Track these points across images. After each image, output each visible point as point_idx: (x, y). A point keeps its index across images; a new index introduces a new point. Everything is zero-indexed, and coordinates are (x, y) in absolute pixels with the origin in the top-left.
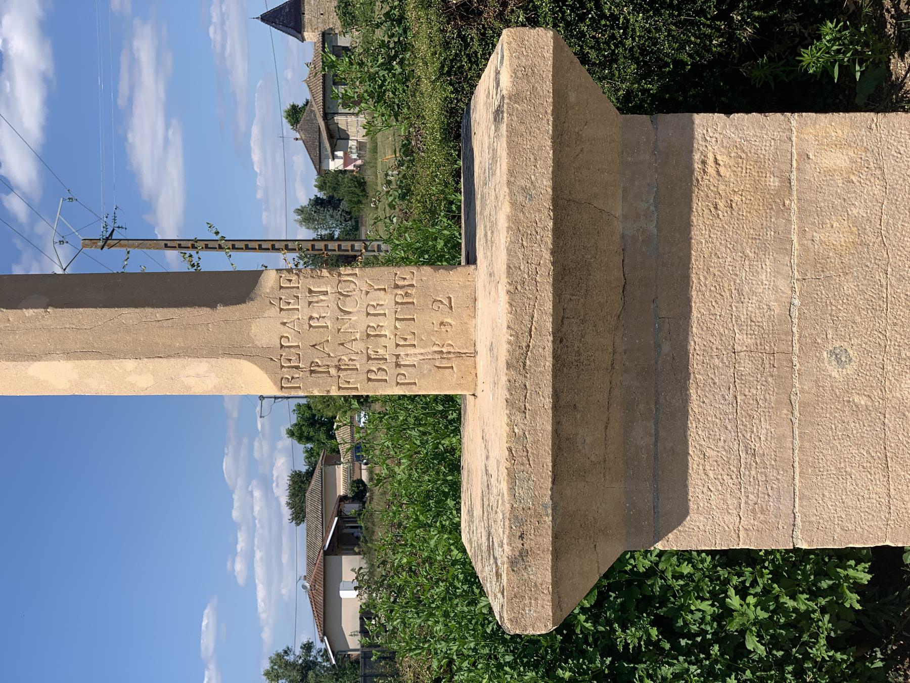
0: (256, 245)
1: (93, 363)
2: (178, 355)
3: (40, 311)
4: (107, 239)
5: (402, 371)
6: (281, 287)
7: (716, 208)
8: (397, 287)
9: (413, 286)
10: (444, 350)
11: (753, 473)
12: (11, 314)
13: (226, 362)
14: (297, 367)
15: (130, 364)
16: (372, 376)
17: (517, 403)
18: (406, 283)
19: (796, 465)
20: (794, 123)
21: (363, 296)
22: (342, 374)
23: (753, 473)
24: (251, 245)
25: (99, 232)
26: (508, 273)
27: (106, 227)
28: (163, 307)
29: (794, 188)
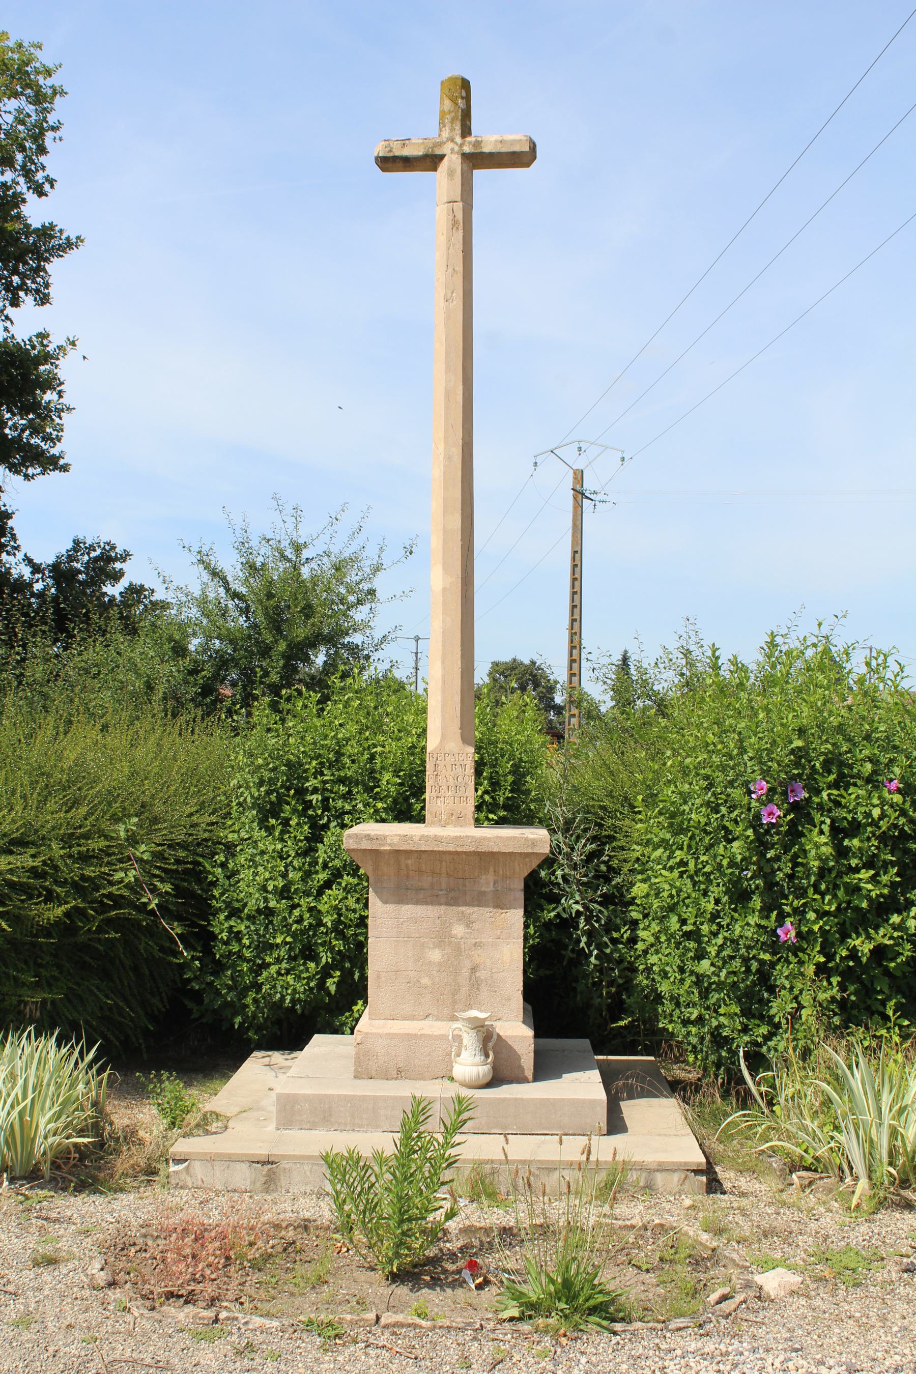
0: (577, 616)
1: (440, 685)
4: (583, 494)
15: (440, 698)
17: (423, 838)
24: (577, 611)
25: (589, 485)
27: (595, 493)
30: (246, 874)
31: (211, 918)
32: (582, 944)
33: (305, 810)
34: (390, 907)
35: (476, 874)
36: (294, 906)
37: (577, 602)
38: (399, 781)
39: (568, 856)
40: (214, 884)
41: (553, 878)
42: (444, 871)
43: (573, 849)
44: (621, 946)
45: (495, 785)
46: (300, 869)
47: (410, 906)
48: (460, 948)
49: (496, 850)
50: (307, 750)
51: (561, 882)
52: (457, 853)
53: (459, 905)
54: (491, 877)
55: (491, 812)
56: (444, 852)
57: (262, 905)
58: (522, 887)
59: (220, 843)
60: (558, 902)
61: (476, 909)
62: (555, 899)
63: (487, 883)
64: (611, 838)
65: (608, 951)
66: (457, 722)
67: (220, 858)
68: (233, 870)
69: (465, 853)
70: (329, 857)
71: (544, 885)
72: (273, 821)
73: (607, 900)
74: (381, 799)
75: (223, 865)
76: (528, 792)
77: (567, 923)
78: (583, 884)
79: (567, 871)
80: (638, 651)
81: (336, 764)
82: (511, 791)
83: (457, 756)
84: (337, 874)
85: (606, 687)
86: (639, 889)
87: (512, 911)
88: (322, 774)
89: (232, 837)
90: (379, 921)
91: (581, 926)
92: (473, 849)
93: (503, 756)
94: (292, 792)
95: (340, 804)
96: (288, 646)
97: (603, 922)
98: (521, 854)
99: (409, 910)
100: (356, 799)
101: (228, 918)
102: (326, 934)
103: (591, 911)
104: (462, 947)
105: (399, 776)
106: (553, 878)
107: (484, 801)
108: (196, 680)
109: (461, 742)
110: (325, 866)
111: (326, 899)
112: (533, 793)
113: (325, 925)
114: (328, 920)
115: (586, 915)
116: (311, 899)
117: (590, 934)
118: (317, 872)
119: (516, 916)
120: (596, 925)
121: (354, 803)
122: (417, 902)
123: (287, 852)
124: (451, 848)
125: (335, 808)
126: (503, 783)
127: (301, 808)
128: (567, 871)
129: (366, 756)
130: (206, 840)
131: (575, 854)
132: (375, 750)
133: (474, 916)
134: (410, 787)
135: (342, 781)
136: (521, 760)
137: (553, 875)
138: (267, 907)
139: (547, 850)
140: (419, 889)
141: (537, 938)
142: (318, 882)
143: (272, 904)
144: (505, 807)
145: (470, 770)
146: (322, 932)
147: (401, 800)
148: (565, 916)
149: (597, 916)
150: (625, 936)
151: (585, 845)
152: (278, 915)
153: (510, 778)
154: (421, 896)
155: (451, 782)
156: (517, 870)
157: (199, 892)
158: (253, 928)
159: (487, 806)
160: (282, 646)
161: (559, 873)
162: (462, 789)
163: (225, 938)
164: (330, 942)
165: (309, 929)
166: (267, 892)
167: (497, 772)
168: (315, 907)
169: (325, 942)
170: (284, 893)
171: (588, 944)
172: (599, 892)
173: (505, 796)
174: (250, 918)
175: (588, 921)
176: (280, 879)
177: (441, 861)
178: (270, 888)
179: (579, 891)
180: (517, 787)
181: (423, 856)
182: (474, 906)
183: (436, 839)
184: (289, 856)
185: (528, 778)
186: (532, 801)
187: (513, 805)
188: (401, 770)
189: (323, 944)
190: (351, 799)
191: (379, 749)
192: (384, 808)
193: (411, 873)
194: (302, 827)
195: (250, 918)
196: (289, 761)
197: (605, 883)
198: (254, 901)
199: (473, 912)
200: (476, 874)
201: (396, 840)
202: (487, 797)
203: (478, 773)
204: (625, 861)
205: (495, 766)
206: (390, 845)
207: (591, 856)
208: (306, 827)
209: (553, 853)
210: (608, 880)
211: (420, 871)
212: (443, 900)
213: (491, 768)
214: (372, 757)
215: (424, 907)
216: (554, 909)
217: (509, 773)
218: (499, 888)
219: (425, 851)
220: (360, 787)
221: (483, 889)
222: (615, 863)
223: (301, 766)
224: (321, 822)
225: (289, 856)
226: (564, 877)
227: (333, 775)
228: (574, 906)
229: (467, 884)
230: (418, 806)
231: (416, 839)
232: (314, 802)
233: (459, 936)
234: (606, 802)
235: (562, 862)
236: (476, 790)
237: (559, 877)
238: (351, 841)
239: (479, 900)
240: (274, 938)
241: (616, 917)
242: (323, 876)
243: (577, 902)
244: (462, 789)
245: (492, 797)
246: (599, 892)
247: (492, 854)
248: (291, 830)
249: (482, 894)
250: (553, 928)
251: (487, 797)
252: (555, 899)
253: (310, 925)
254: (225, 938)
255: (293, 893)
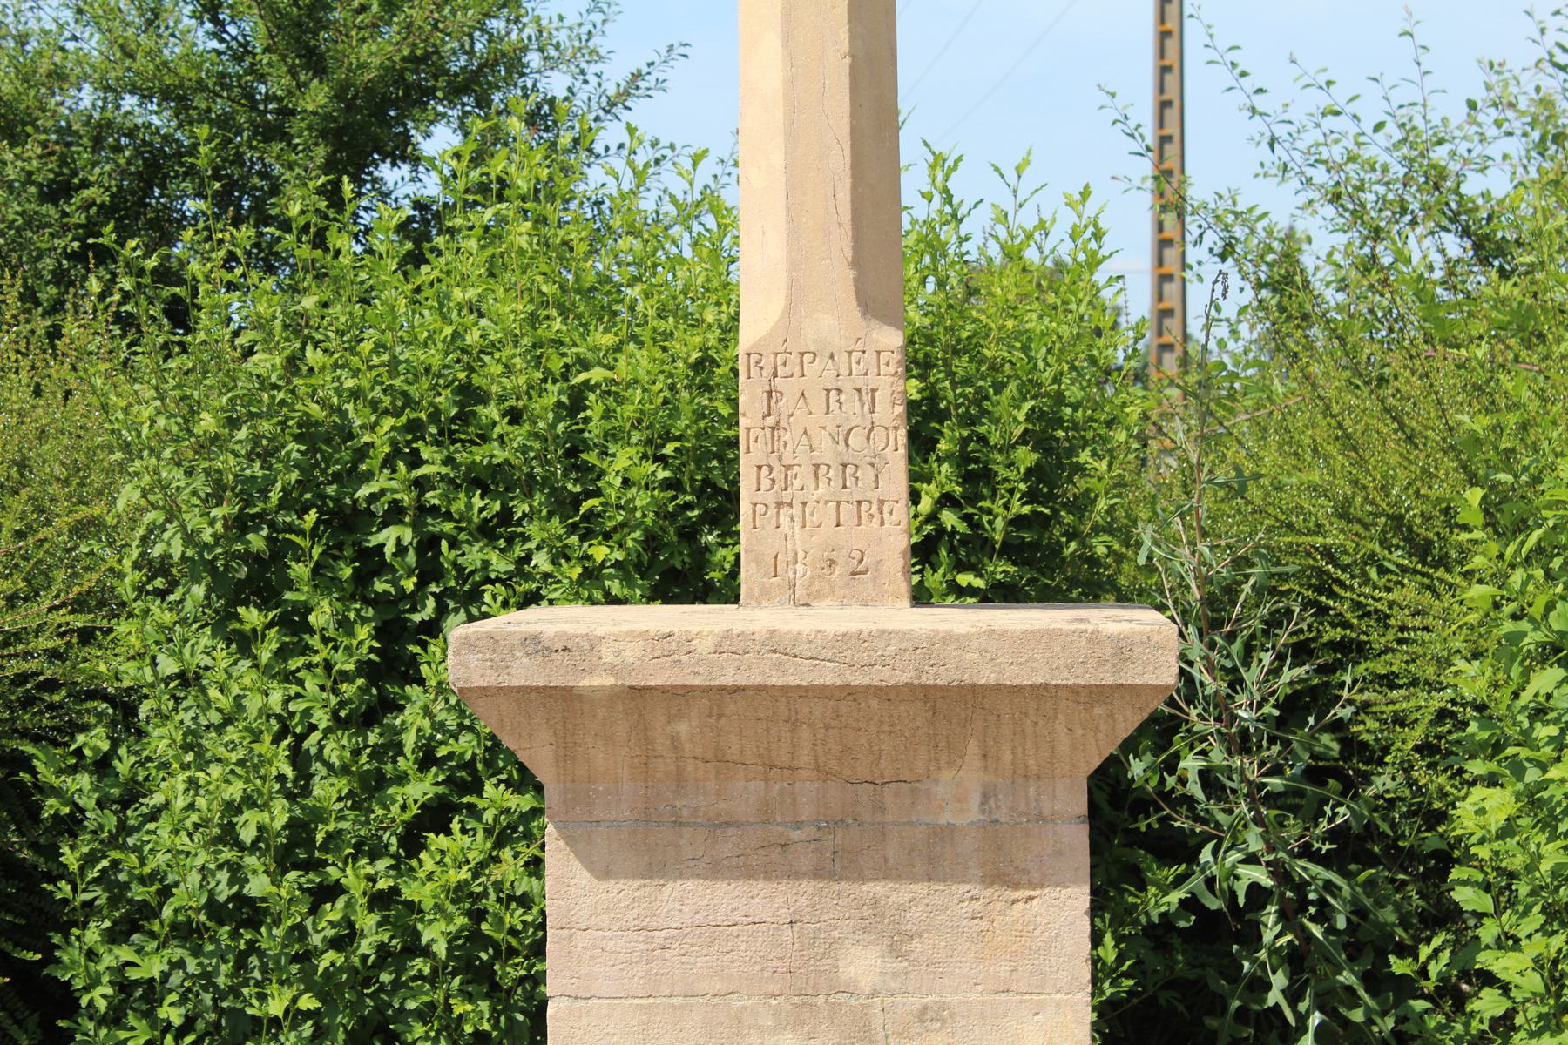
0: (1171, 25)
2: (790, 220)
3: (846, 47)
5: (772, 511)
6: (879, 353)
7: (972, 899)
8: (881, 502)
9: (882, 524)
10: (799, 567)
11: (642, 947)
12: (842, 11)
13: (782, 282)
14: (775, 375)
15: (778, 160)
16: (765, 471)
17: (727, 644)
18: (886, 515)
19: (652, 1000)
20: (1079, 996)
21: (868, 459)
22: (768, 431)
23: (642, 947)
26: (883, 632)
28: (852, 201)
29: (997, 997)
30: (172, 790)
31: (57, 939)
32: (1274, 997)
33: (362, 579)
34: (622, 890)
35: (920, 766)
36: (328, 892)
37: (1171, 58)
38: (663, 474)
39: (1222, 709)
40: (71, 824)
41: (1171, 781)
42: (805, 757)
43: (1236, 683)
44: (1419, 1005)
45: (977, 478)
46: (345, 770)
47: (689, 884)
48: (867, 1028)
49: (987, 677)
50: (365, 384)
51: (1199, 794)
52: (850, 692)
53: (862, 878)
54: (971, 776)
55: (962, 566)
56: (804, 692)
57: (224, 893)
58: (1082, 807)
59: (97, 694)
60: (1192, 857)
61: (920, 888)
62: (1180, 850)
63: (957, 795)
64: (1353, 650)
65: (1357, 1016)
66: (841, 243)
67: (95, 740)
68: (133, 780)
69: (880, 692)
70: (440, 727)
71: (1143, 805)
72: (252, 617)
73: (1349, 849)
74: (607, 536)
75: (103, 766)
76: (1082, 505)
77: (1222, 928)
78: (1272, 799)
79: (1218, 756)
80: (1414, 73)
81: (459, 426)
82: (1031, 497)
83: (842, 359)
84: (465, 779)
85: (1313, 194)
86: (1481, 811)
87: (1050, 892)
88: (415, 461)
89: (131, 673)
90: (582, 940)
91: (1268, 936)
92: (903, 678)
93: (999, 387)
94: (311, 517)
95: (474, 555)
96: (339, 95)
97: (1341, 923)
98: (1075, 690)
99: (686, 899)
100: (526, 538)
101: (115, 936)
102: (433, 979)
103: (1301, 887)
104: (877, 1022)
105: (662, 460)
106: (1171, 781)
107: (941, 530)
108: (65, 214)
109: (856, 312)
110: (427, 760)
111: (429, 865)
112: (1102, 504)
113: (426, 952)
114: (435, 935)
115: (1282, 900)
116: (383, 864)
117: (1297, 960)
118: (402, 779)
119: (1064, 910)
120: (1317, 931)
121: (518, 551)
122: (715, 871)
123: (307, 713)
124: (827, 676)
125: (460, 569)
126: (1004, 473)
127: (347, 572)
128: (1218, 756)
129: (554, 393)
130: (51, 685)
131: (1242, 698)
132: (583, 377)
133: (915, 914)
134: (699, 493)
135: (480, 480)
136: (1059, 399)
137: (1172, 771)
138: (238, 898)
139: (1167, 676)
140: (720, 825)
141: (1127, 975)
142: (404, 808)
143: (258, 886)
144: (1010, 550)
145: (890, 415)
146: (420, 976)
147: (672, 535)
148: (1213, 903)
149: (1322, 903)
150: (1434, 970)
151: (1275, 672)
152: (277, 922)
153: (1026, 457)
154: (727, 849)
155: (827, 452)
156: (1063, 747)
157: (26, 854)
158: (192, 966)
159: (952, 550)
160: (317, 97)
161: (1190, 764)
162: (866, 474)
163: (102, 1005)
164: (448, 1008)
165: (380, 965)
166: (241, 847)
167: (983, 440)
168: (395, 891)
169: (432, 1006)
170: (296, 849)
171: (1293, 996)
172: (1324, 825)
173: (1008, 495)
174: (185, 932)
175: (1287, 917)
176: (280, 804)
177: (794, 724)
178: (247, 835)
179: (1258, 820)
180: (1046, 479)
181: (732, 707)
182: (914, 879)
183: (775, 645)
184: (313, 728)
185: (1084, 457)
186: (1096, 530)
187: (1034, 546)
188: (667, 437)
189: (424, 1015)
190: (510, 540)
191: (596, 375)
192: (617, 565)
193: (690, 766)
194: (351, 634)
195: (185, 932)
196: (307, 422)
197: (1344, 794)
198: (194, 878)
199: (910, 898)
200: (920, 766)
201: (632, 652)
202: (949, 519)
203: (921, 443)
204: (1400, 720)
205: (972, 421)
206: (612, 670)
207: (1294, 708)
208: (363, 632)
209: (1171, 702)
210: (1350, 788)
211: (720, 761)
212: (805, 860)
213: (962, 425)
214: (575, 403)
215: (740, 887)
216: (1179, 881)
217: (1023, 439)
218: (1002, 815)
219: (737, 690)
220: (538, 498)
221: (946, 818)
222: (1367, 730)
223: (351, 436)
224: (417, 618)
225: (313, 728)
226: (1206, 776)
227: (448, 461)
228: (1242, 870)
229: (889, 800)
230: (724, 555)
231: (704, 646)
232: (389, 550)
233: (865, 985)
234: (1335, 537)
235: (1199, 727)
236: (915, 497)
237: (1193, 776)
238: (473, 659)
239: (933, 858)
240: (262, 997)
241: (1380, 904)
242: (421, 789)
243: (1252, 859)
244: (866, 474)
245: (967, 518)
246: (1324, 825)
247: (972, 695)
248: (315, 642)
249: (946, 833)
250: (1177, 942)
251: (949, 519)
252: (1180, 850)
253: (382, 948)
254: (102, 1005)
255: (324, 847)
